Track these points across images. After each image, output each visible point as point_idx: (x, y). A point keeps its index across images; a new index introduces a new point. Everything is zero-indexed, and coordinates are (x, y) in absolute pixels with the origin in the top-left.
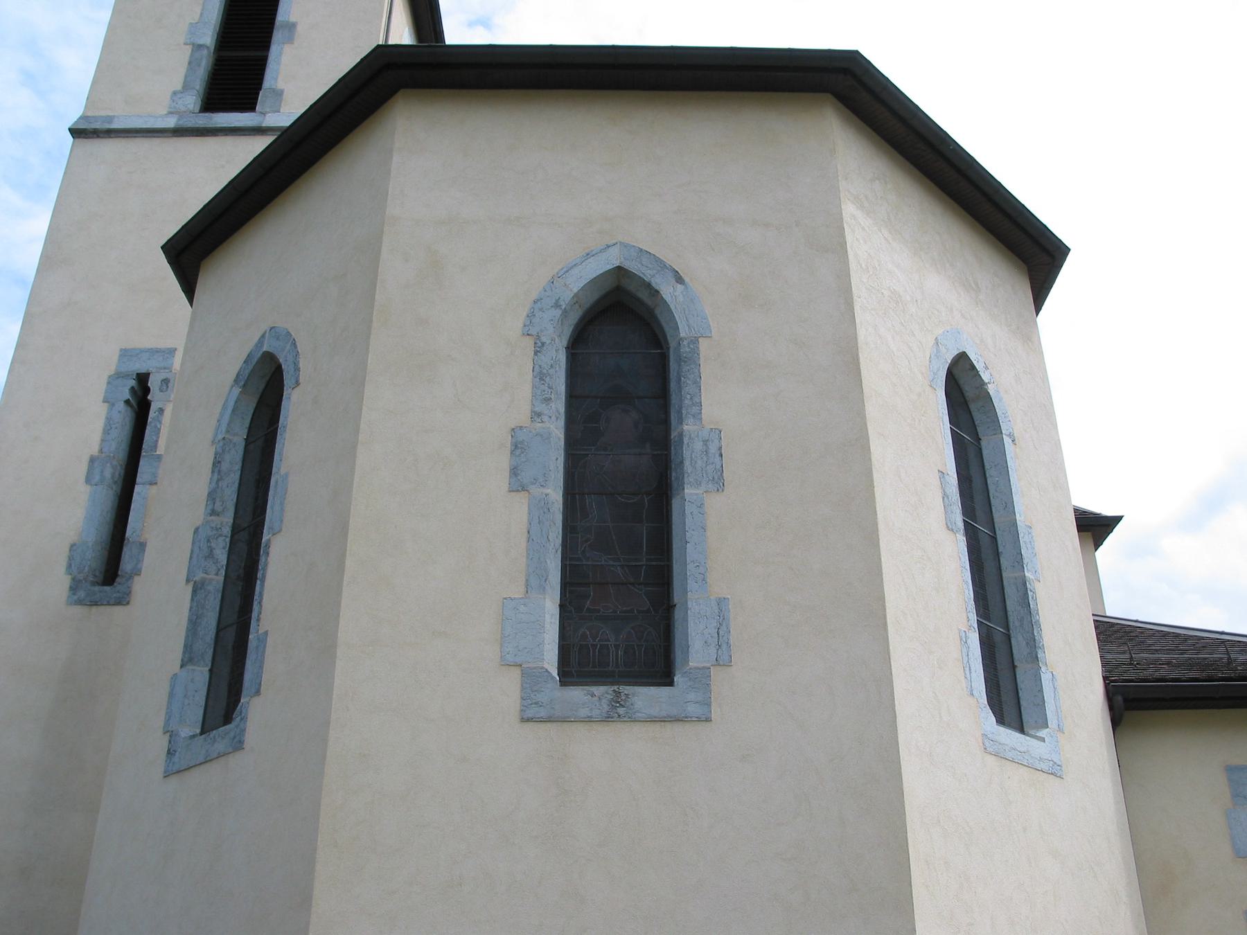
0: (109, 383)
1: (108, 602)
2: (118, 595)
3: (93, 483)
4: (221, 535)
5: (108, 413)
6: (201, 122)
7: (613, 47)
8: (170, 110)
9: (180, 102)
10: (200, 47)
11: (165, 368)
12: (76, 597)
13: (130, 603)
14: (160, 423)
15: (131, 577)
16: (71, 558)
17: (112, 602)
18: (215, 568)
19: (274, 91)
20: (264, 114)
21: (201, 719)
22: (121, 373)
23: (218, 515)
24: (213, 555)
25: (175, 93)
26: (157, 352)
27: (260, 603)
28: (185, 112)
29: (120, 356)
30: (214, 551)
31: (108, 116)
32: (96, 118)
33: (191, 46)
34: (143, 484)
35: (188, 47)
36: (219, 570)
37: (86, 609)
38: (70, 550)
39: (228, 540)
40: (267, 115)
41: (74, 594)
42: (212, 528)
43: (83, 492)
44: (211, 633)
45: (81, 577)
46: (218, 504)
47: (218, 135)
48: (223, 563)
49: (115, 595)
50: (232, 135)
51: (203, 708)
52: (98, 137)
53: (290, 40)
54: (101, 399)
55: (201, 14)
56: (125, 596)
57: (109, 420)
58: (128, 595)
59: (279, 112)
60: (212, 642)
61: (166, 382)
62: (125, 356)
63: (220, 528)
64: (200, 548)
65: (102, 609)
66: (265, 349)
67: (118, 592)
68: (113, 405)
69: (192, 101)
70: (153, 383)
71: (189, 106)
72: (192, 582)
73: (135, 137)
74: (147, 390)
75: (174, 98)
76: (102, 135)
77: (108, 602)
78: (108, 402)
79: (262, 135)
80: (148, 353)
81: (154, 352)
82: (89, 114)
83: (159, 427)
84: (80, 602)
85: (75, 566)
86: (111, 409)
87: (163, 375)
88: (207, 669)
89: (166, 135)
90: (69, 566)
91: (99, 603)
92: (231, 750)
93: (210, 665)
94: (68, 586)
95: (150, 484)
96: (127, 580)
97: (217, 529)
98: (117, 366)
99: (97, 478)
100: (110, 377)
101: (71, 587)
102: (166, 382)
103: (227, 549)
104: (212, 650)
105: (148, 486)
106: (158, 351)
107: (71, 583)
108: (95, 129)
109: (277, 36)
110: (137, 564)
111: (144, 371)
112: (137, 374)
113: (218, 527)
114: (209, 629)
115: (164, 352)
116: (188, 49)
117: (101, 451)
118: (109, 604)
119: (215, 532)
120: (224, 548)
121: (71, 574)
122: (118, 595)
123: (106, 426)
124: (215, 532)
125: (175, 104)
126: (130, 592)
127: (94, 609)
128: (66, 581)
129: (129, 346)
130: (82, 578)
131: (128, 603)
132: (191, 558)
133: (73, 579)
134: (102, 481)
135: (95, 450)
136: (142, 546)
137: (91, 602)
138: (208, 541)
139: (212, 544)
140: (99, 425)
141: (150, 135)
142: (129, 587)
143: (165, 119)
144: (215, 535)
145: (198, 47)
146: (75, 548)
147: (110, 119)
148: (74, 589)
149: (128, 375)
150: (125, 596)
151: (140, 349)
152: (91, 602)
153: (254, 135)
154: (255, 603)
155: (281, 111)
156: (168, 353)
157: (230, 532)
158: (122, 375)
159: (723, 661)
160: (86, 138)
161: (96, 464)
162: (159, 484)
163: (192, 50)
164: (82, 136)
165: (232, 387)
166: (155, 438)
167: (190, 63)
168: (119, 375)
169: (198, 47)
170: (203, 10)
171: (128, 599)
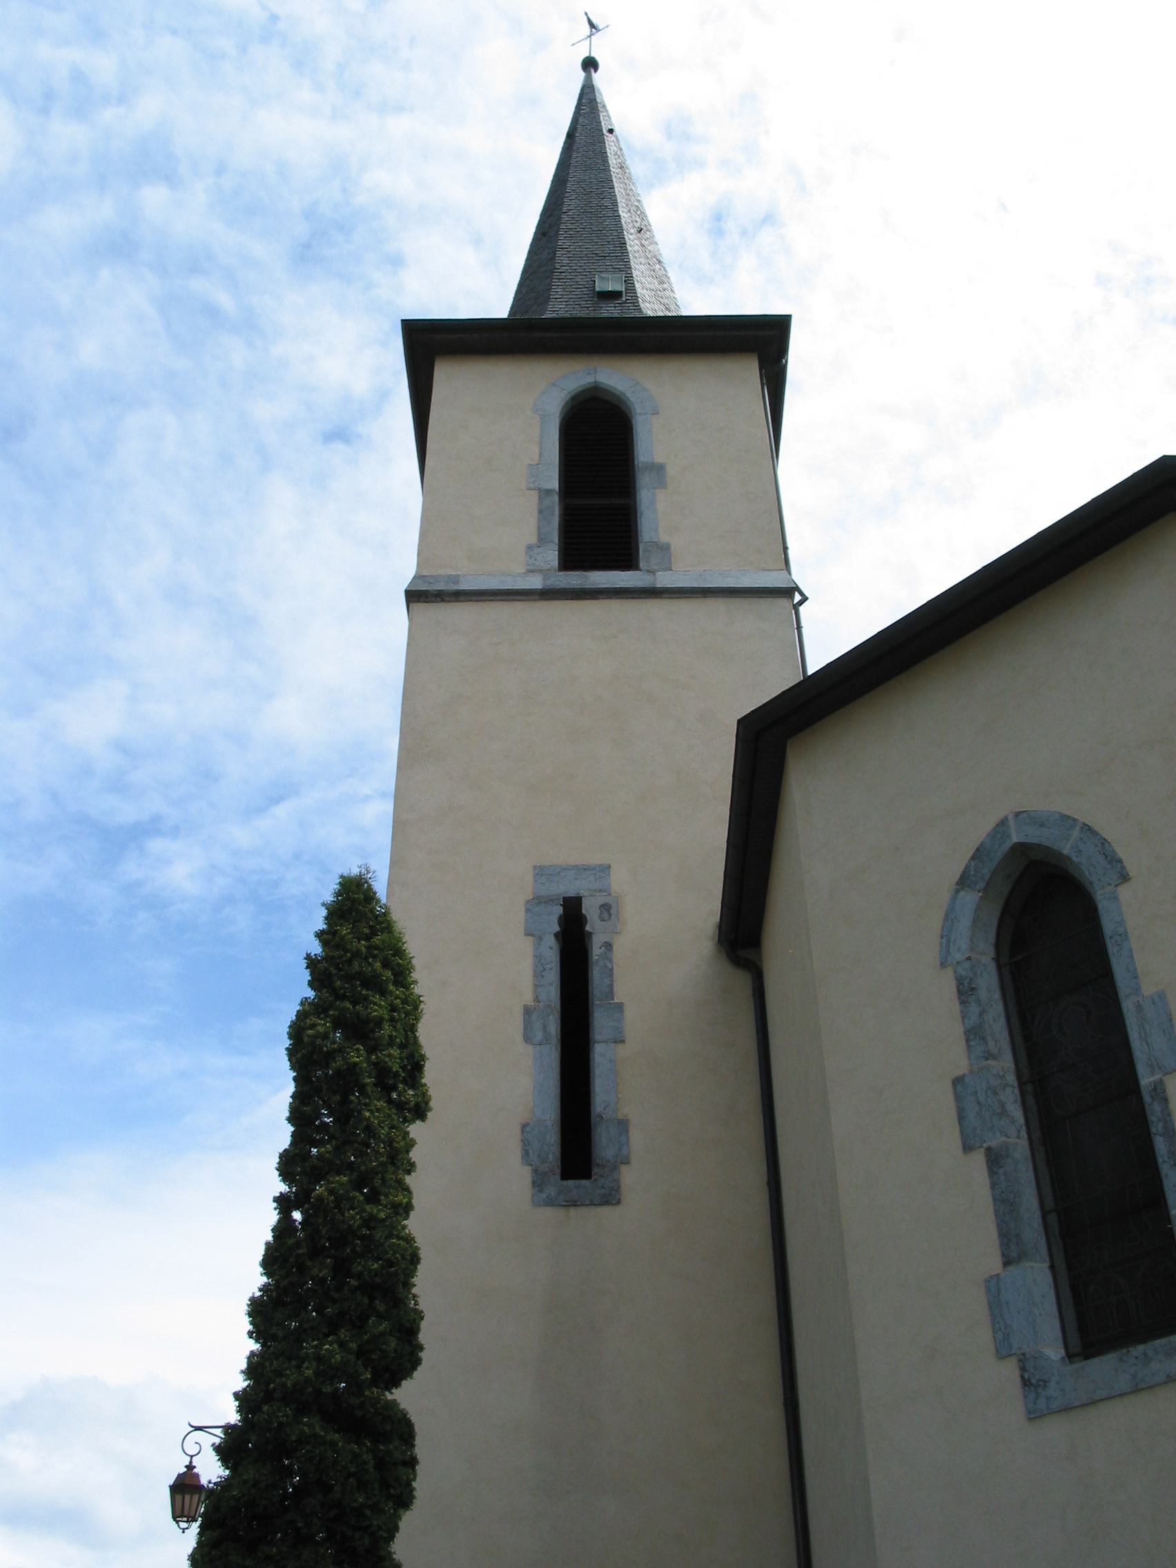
52: (443, 601)
76: (447, 599)
99: (539, 1035)
118: (592, 1204)
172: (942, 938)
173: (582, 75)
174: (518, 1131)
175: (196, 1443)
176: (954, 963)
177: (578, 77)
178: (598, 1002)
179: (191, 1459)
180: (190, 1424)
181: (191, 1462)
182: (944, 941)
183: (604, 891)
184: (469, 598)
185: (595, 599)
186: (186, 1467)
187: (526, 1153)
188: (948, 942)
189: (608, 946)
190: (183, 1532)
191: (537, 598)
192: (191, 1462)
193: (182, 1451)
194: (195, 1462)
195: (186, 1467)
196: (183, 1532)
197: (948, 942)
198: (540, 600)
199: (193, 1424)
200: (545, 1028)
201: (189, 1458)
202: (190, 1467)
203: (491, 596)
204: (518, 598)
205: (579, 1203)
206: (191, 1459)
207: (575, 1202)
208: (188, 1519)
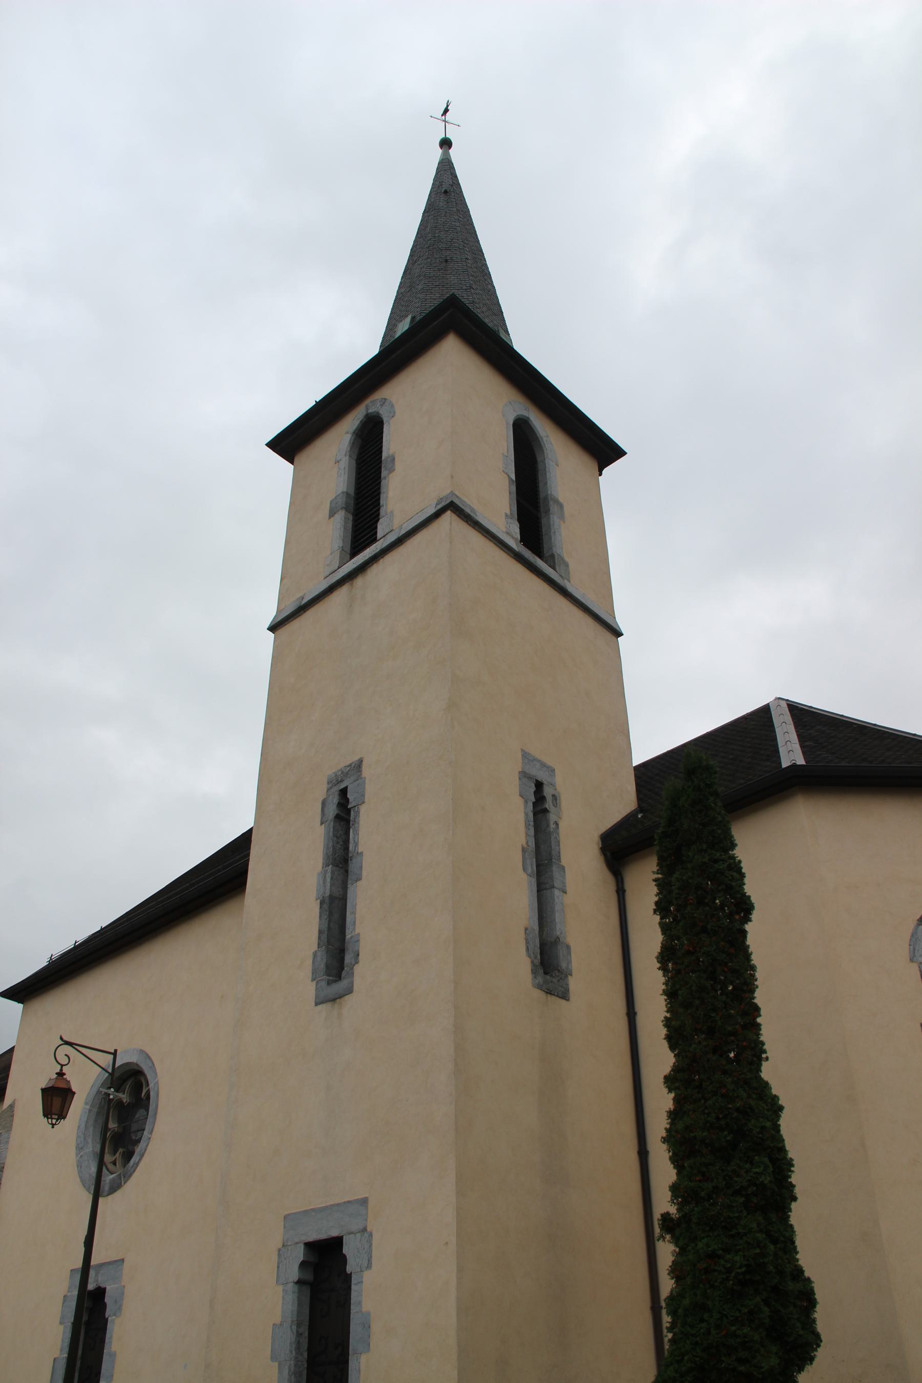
16: (527, 942)
47: (539, 578)
52: (467, 522)
73: (491, 540)
76: (469, 522)
99: (529, 871)
101: (532, 970)
118: (558, 996)
137: (548, 990)
149: (531, 778)
160: (458, 516)
172: (910, 945)
173: (440, 151)
174: (523, 932)
175: (66, 1055)
176: (919, 962)
177: (437, 153)
178: (554, 860)
179: (62, 1068)
180: (61, 1038)
181: (61, 1070)
182: (912, 947)
183: (553, 786)
184: (480, 530)
185: (538, 577)
186: (57, 1074)
187: (527, 949)
188: (914, 949)
189: (557, 824)
190: (53, 1127)
191: (512, 556)
192: (61, 1070)
193: (56, 1063)
194: (65, 1069)
195: (57, 1074)
196: (53, 1127)
197: (914, 949)
198: (513, 558)
199: (65, 1038)
200: (532, 868)
201: (59, 1067)
202: (61, 1074)
203: (492, 537)
204: (504, 549)
205: (552, 993)
206: (62, 1068)
207: (551, 991)
208: (58, 1117)
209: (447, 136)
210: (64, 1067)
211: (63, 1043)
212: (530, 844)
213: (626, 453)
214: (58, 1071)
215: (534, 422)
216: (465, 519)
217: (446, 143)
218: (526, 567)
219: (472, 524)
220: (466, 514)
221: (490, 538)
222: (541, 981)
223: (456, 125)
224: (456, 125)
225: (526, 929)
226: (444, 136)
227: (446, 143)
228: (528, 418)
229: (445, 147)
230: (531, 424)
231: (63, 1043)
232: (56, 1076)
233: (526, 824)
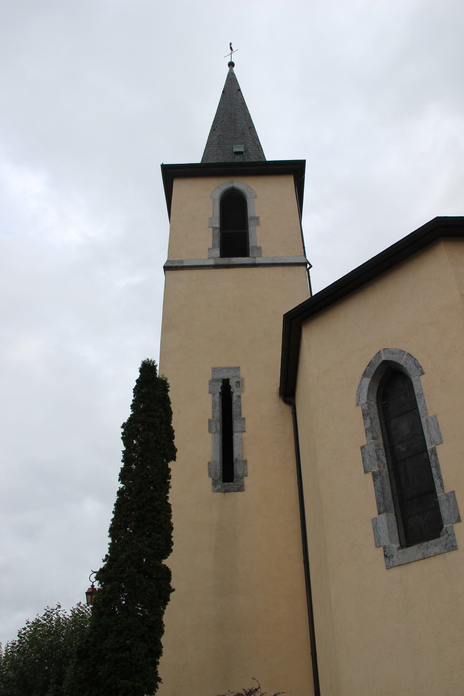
0: (209, 384)
1: (234, 490)
2: (238, 486)
3: (213, 433)
4: (380, 449)
5: (212, 399)
6: (226, 262)
7: (427, 224)
8: (209, 257)
9: (213, 253)
10: (216, 228)
11: (236, 376)
12: (216, 488)
13: (245, 490)
14: (240, 402)
15: (242, 478)
16: (209, 469)
17: (235, 490)
18: (383, 465)
19: (256, 247)
20: (254, 258)
21: (398, 538)
22: (215, 379)
23: (376, 439)
24: (380, 458)
25: (209, 249)
26: (231, 369)
27: (440, 477)
28: (216, 257)
29: (212, 371)
30: (380, 456)
31: (180, 260)
32: (175, 261)
33: (212, 228)
34: (238, 432)
35: (210, 228)
36: (384, 466)
37: (222, 494)
38: (208, 465)
39: (384, 451)
40: (257, 258)
41: (215, 487)
42: (376, 445)
43: (209, 437)
44: (390, 496)
45: (217, 478)
46: (374, 434)
47: (235, 268)
48: (384, 462)
49: (236, 487)
50: (242, 268)
51: (397, 533)
52: (177, 270)
53: (258, 224)
54: (208, 392)
55: (213, 214)
56: (242, 487)
57: (214, 401)
58: (243, 486)
59: (262, 257)
60: (392, 501)
61: (238, 383)
62: (215, 371)
63: (379, 445)
64: (370, 455)
65: (230, 493)
66: (383, 358)
67: (238, 485)
68: (214, 394)
69: (217, 252)
70: (232, 383)
71: (217, 255)
72: (371, 473)
73: (195, 269)
74: (229, 387)
75: (210, 251)
76: (179, 269)
77: (234, 490)
78: (211, 393)
79: (256, 267)
80: (226, 370)
81: (229, 369)
82: (171, 259)
83: (240, 404)
84: (219, 491)
85: (212, 473)
86: (214, 396)
87: (236, 380)
88: (394, 514)
89: (210, 268)
90: (210, 473)
91: (229, 491)
92: (445, 551)
93: (394, 512)
94: (211, 483)
95: (242, 432)
96: (241, 479)
97: (378, 446)
98: (212, 376)
99: (214, 430)
100: (209, 381)
101: (212, 484)
102: (238, 383)
103: (385, 455)
104: (393, 504)
105: (241, 433)
106: (231, 368)
107: (212, 481)
108: (176, 266)
109: (251, 224)
110: (244, 471)
111: (226, 378)
112: (223, 379)
113: (378, 445)
114: (389, 494)
115: (234, 368)
116: (211, 230)
117: (213, 417)
118: (234, 491)
119: (377, 448)
120: (383, 455)
121: (212, 477)
122: (238, 486)
123: (213, 405)
124: (377, 448)
125: (210, 254)
126: (244, 485)
127: (227, 494)
128: (209, 481)
129: (216, 366)
130: (217, 479)
131: (244, 490)
132: (363, 461)
133: (213, 479)
134: (217, 431)
135: (210, 417)
136: (245, 462)
137: (225, 490)
138: (376, 452)
139: (378, 453)
140: (209, 405)
141: (203, 268)
142: (243, 483)
143: (208, 261)
144: (378, 448)
145: (215, 229)
146: (210, 464)
147: (182, 261)
148: (215, 483)
149: (219, 380)
150: (242, 487)
151: (221, 368)
152: (225, 490)
153: (252, 267)
154: (436, 479)
155: (262, 256)
156: (236, 369)
157: (383, 447)
158: (215, 380)
159: (375, 522)
160: (172, 270)
161: (212, 423)
162: (246, 432)
163: (213, 230)
164: (170, 269)
165: (362, 378)
166: (239, 410)
167: (213, 236)
168: (213, 381)
169: (215, 229)
170: (213, 212)
171: (243, 488)
179: (93, 583)
180: (92, 571)
181: (93, 584)
182: (358, 396)
184: (187, 269)
186: (91, 586)
188: (359, 396)
189: (239, 397)
192: (93, 584)
195: (91, 586)
197: (359, 396)
198: (213, 269)
206: (93, 583)
209: (232, 61)
210: (94, 583)
211: (93, 572)
212: (215, 416)
213: (305, 160)
214: (92, 585)
215: (237, 186)
216: (176, 269)
217: (231, 65)
218: (223, 268)
219: (181, 269)
220: (174, 267)
221: (195, 268)
222: (219, 488)
223: (226, 56)
224: (226, 56)
225: (209, 463)
226: (230, 61)
227: (231, 65)
228: (233, 186)
229: (231, 66)
230: (236, 188)
231: (93, 572)
232: (91, 587)
233: (212, 407)
